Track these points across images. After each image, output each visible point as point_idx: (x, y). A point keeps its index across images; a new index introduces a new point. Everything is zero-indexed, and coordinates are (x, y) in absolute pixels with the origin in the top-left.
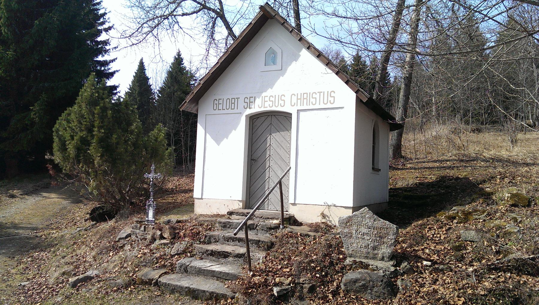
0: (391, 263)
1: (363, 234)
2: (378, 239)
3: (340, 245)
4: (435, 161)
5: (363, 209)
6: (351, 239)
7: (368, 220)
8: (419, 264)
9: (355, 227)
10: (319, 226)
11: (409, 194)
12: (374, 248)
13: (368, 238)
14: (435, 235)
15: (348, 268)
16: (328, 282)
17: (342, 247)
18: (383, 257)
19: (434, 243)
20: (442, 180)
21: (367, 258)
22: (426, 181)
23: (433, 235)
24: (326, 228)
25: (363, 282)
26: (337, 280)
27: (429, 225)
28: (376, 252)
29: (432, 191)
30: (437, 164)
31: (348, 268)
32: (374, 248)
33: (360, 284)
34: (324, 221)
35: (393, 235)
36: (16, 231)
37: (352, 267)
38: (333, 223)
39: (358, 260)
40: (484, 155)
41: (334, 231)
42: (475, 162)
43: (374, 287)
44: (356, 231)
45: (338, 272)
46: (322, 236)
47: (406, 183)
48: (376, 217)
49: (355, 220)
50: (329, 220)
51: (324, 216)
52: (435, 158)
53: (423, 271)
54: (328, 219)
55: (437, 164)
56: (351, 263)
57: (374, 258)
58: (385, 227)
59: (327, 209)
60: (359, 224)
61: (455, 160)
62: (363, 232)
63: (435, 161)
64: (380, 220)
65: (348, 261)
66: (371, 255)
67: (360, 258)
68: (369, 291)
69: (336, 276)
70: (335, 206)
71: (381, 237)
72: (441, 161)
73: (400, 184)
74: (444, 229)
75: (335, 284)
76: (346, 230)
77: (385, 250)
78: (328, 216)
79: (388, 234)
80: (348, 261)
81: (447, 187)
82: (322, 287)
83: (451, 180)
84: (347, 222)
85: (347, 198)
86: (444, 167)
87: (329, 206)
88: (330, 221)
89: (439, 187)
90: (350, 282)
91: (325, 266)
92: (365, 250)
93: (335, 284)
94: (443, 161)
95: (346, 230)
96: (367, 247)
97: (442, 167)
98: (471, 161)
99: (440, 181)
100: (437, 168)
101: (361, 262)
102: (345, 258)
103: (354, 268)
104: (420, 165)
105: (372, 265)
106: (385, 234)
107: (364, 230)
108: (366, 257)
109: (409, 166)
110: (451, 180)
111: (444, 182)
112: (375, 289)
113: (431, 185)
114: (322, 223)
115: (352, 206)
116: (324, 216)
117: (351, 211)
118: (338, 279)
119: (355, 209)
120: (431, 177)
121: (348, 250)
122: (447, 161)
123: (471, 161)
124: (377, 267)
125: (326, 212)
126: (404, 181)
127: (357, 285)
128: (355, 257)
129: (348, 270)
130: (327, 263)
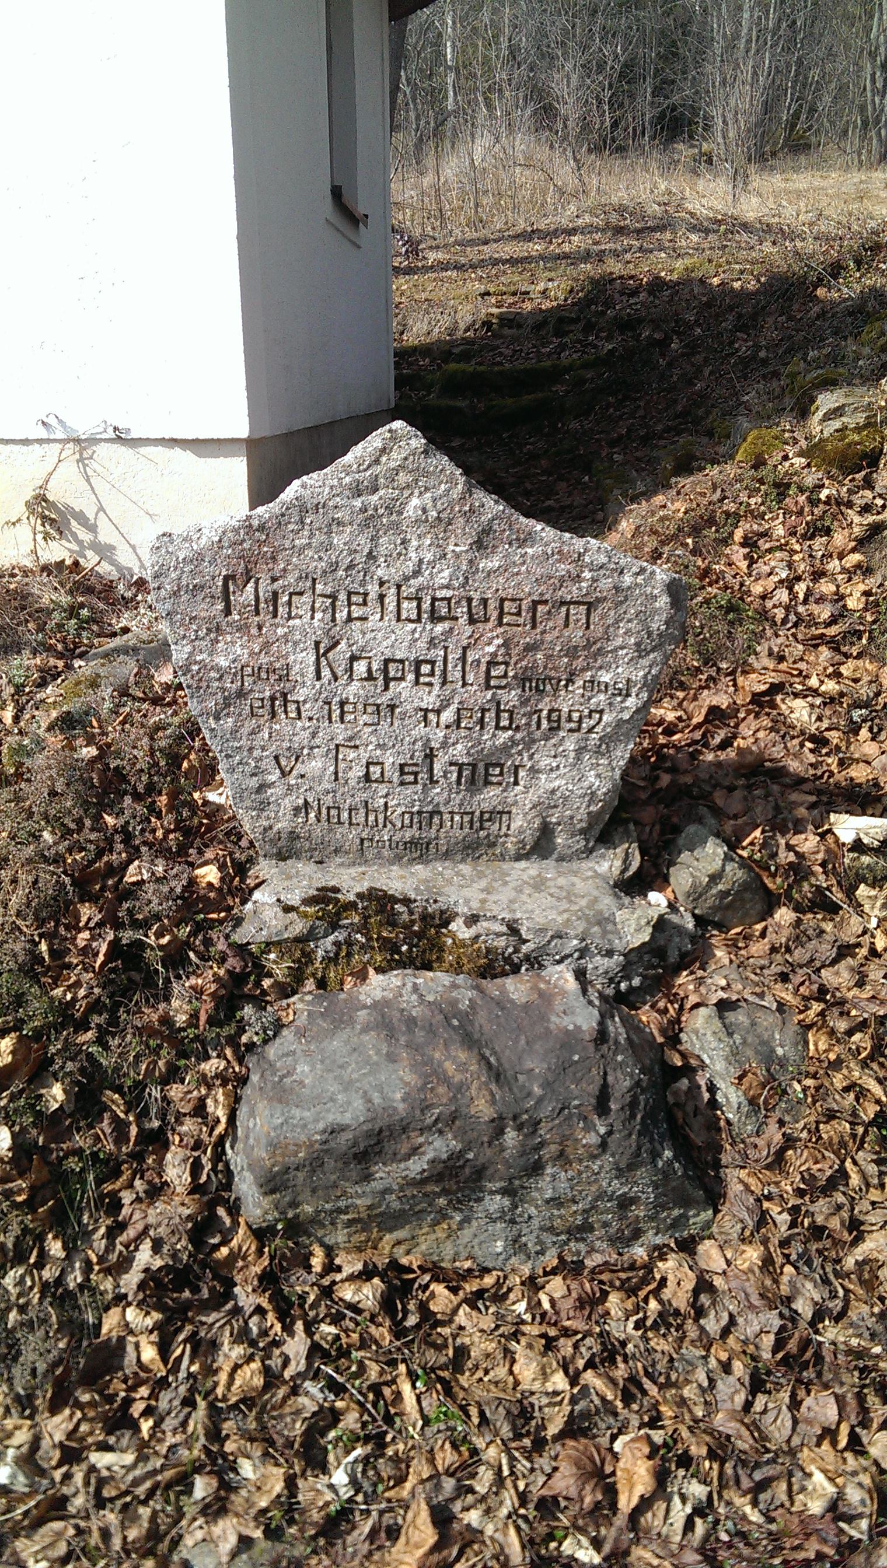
0: (609, 863)
1: (386, 673)
2: (511, 697)
3: (183, 762)
4: (527, 236)
5: (375, 440)
6: (282, 726)
7: (421, 548)
8: (808, 842)
9: (307, 621)
10: (22, 599)
11: (469, 367)
12: (477, 773)
13: (430, 700)
14: (801, 588)
15: (279, 967)
16: (110, 1169)
17: (208, 774)
18: (546, 832)
19: (815, 643)
20: (600, 293)
21: (418, 850)
22: (528, 306)
23: (789, 584)
24: (72, 611)
25: (440, 1146)
26: (189, 1126)
27: (735, 518)
28: (489, 797)
29: (563, 347)
30: (537, 247)
31: (279, 967)
32: (477, 773)
33: (416, 1166)
34: (56, 552)
35: (641, 651)
36: (540, 395)
37: (308, 957)
38: (125, 558)
39: (351, 881)
40: (690, 207)
41: (134, 623)
42: (668, 235)
43: (536, 1169)
44: (322, 652)
45: (186, 1047)
46: (48, 676)
47: (446, 321)
48: (491, 506)
49: (305, 554)
50: (96, 546)
51: (49, 514)
52: (522, 225)
53: (837, 896)
54: (84, 535)
55: (537, 247)
56: (299, 927)
57: (478, 844)
58: (573, 592)
59: (70, 470)
60: (345, 598)
61: (598, 229)
62: (381, 649)
63: (527, 236)
64: (526, 539)
65: (273, 904)
66: (453, 830)
67: (361, 853)
68: (496, 1203)
69: (175, 1091)
70: (120, 438)
71: (532, 683)
72: (548, 235)
73: (420, 330)
74: (840, 539)
75: (176, 1170)
76: (232, 652)
77: (571, 776)
78: (81, 518)
79: (594, 651)
80: (273, 904)
81: (628, 325)
82: (55, 1248)
83: (634, 293)
84: (239, 575)
85: (202, 371)
86: (566, 256)
87: (83, 444)
88: (105, 551)
89: (589, 328)
90: (315, 1163)
91: (66, 1017)
92: (402, 800)
93: (176, 1170)
94: (556, 233)
95: (232, 652)
96: (418, 769)
97: (558, 257)
98: (652, 229)
99: (588, 301)
100: (542, 257)
101: (380, 902)
102: (238, 882)
103: (331, 960)
104: (473, 254)
105: (473, 920)
106: (572, 652)
107: (388, 636)
108: (413, 843)
109: (432, 256)
110: (634, 293)
111: (609, 304)
112: (551, 1182)
113: (554, 323)
114: (45, 568)
115: (243, 431)
116: (49, 514)
117: (234, 473)
118: (200, 1110)
119: (281, 455)
120: (550, 290)
121: (263, 806)
122: (573, 232)
123: (652, 229)
124: (513, 930)
125: (68, 489)
126: (435, 314)
127: (385, 1175)
128: (321, 854)
129: (286, 991)
130: (80, 987)
